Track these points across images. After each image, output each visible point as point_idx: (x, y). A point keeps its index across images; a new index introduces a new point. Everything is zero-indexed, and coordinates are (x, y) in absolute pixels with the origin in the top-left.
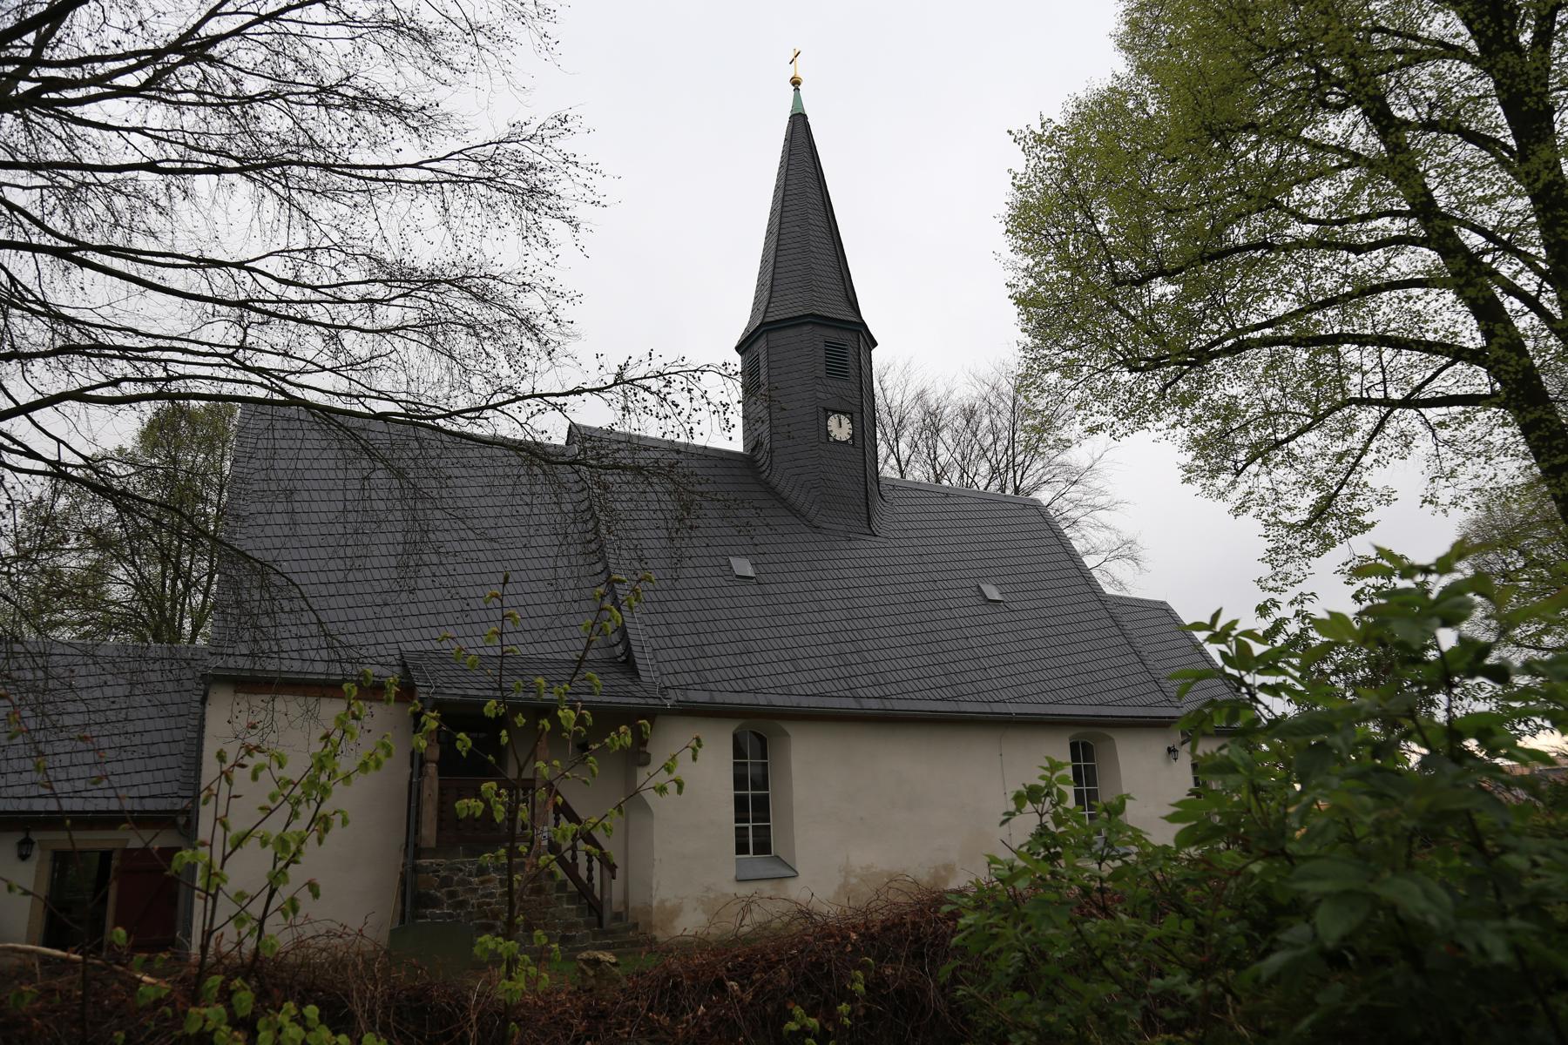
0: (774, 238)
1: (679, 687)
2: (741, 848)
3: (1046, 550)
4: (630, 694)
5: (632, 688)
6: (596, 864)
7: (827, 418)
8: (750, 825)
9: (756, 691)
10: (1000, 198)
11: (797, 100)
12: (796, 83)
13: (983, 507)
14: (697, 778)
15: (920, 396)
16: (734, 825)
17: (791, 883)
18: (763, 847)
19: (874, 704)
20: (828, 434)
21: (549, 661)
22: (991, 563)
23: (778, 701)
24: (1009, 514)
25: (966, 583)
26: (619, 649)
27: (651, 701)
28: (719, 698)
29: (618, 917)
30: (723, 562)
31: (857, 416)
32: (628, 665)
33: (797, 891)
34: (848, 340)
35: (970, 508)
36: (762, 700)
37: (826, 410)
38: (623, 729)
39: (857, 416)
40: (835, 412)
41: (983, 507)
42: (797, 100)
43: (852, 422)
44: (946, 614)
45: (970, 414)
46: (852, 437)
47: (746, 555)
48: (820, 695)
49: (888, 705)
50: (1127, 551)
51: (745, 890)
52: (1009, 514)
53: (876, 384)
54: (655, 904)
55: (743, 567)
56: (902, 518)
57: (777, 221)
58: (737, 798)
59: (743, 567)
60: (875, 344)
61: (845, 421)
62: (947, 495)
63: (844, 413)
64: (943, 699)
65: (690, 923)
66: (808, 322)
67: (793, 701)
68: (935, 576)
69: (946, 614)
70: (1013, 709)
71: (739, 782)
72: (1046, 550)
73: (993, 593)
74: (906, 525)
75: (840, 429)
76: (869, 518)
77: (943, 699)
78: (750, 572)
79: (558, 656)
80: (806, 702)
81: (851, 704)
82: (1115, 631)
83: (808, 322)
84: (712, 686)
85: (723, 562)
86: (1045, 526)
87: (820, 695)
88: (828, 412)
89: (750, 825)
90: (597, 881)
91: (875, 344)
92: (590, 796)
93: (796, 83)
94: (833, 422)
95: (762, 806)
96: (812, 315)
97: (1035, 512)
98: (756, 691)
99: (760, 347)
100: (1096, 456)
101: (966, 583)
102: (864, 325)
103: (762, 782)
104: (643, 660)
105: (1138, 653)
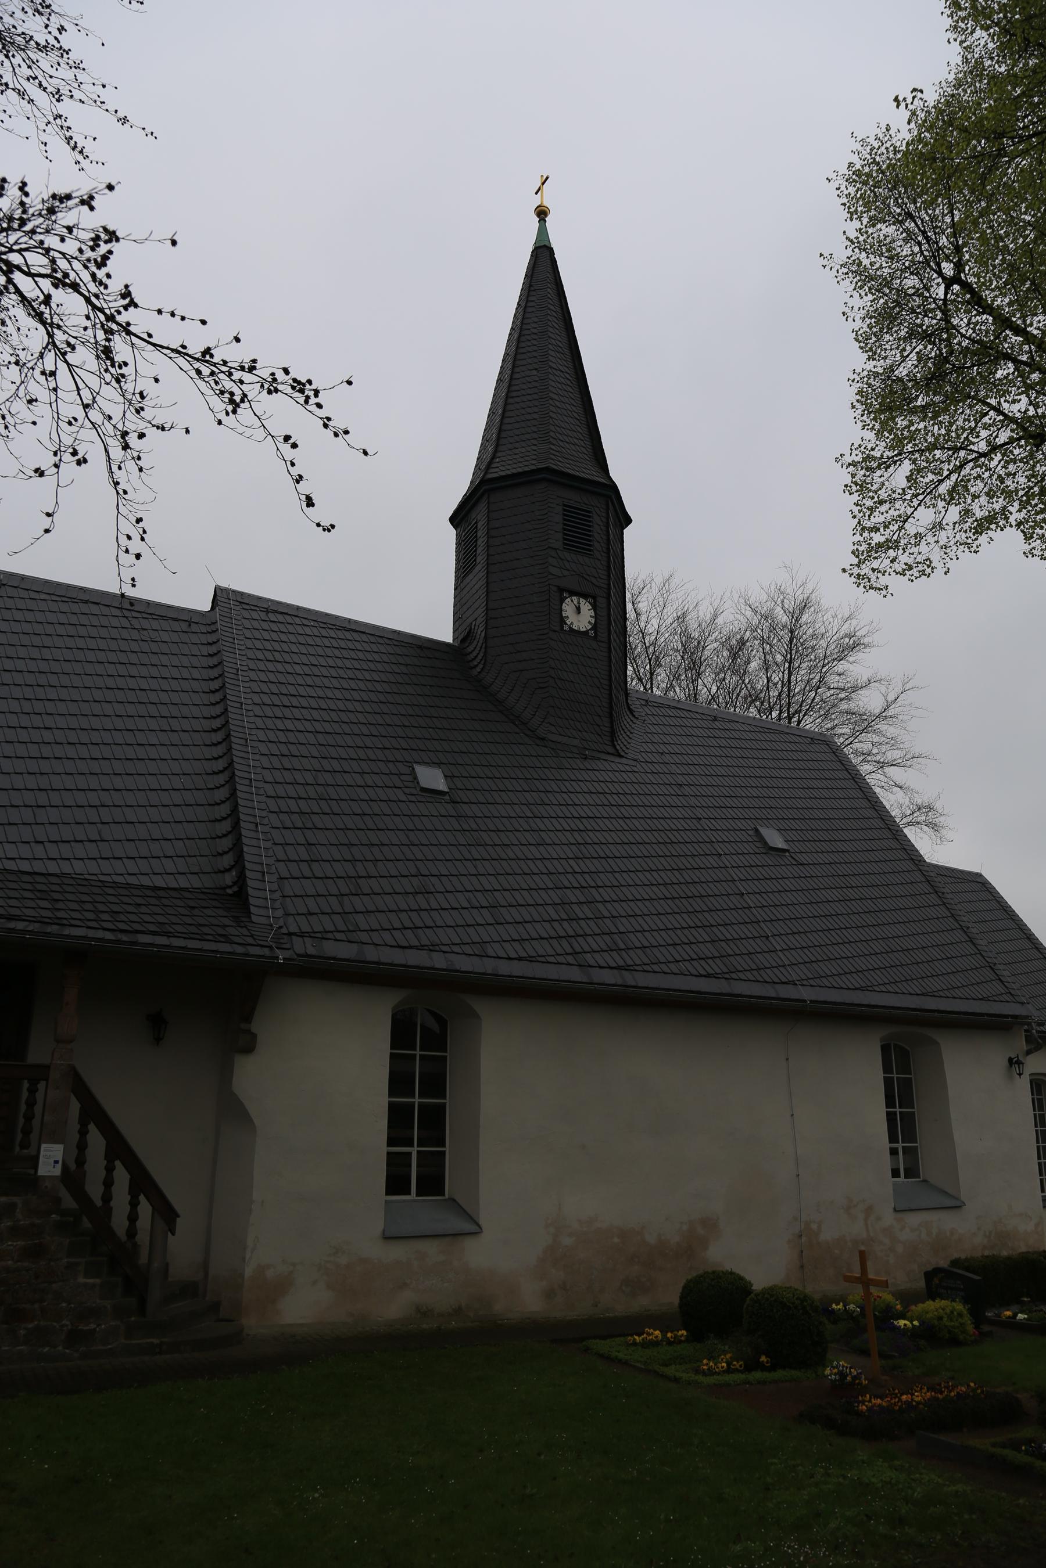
0: (505, 385)
1: (311, 935)
2: (396, 1184)
3: (840, 794)
4: (227, 939)
5: (232, 931)
6: (145, 1208)
7: (562, 601)
8: (414, 1150)
9: (432, 948)
10: (843, 156)
11: (543, 231)
12: (542, 213)
13: (759, 736)
14: (323, 1074)
15: (681, 618)
16: (384, 1149)
17: (469, 1243)
18: (432, 1184)
19: (608, 977)
20: (562, 621)
21: (116, 885)
22: (773, 803)
23: (464, 964)
24: (793, 747)
25: (740, 824)
26: (229, 878)
27: (253, 951)
28: (371, 954)
29: (189, 1290)
30: (407, 770)
31: (602, 602)
32: (237, 899)
33: (481, 1255)
34: (594, 513)
35: (745, 735)
36: (439, 961)
37: (561, 590)
38: (211, 994)
39: (602, 602)
40: (573, 593)
41: (759, 736)
42: (543, 231)
43: (594, 607)
44: (712, 861)
45: (737, 649)
46: (595, 627)
47: (438, 764)
48: (530, 959)
49: (629, 979)
50: (926, 813)
51: (398, 1252)
52: (793, 747)
53: (629, 606)
54: (248, 1272)
55: (432, 778)
56: (656, 739)
57: (510, 365)
58: (888, 1113)
59: (432, 778)
60: (629, 521)
61: (586, 607)
62: (715, 719)
63: (585, 596)
64: (708, 976)
65: (304, 1308)
66: (543, 485)
67: (487, 966)
68: (699, 812)
69: (712, 861)
70: (807, 994)
71: (399, 1083)
72: (840, 794)
73: (776, 840)
74: (662, 748)
75: (580, 616)
76: (613, 734)
77: (708, 976)
78: (442, 785)
79: (132, 880)
80: (505, 968)
81: (574, 974)
82: (933, 899)
83: (543, 485)
84: (364, 937)
85: (404, 769)
86: (838, 766)
87: (530, 959)
88: (565, 592)
89: (414, 1150)
90: (143, 1237)
91: (629, 521)
92: (142, 1093)
93: (542, 213)
94: (568, 608)
95: (434, 1122)
96: (548, 469)
97: (824, 748)
98: (432, 948)
99: (480, 515)
100: (891, 698)
101: (740, 824)
102: (614, 488)
103: (435, 1084)
104: (261, 893)
105: (965, 930)
